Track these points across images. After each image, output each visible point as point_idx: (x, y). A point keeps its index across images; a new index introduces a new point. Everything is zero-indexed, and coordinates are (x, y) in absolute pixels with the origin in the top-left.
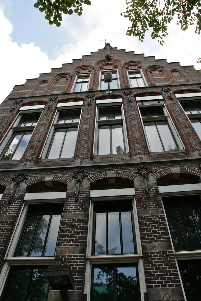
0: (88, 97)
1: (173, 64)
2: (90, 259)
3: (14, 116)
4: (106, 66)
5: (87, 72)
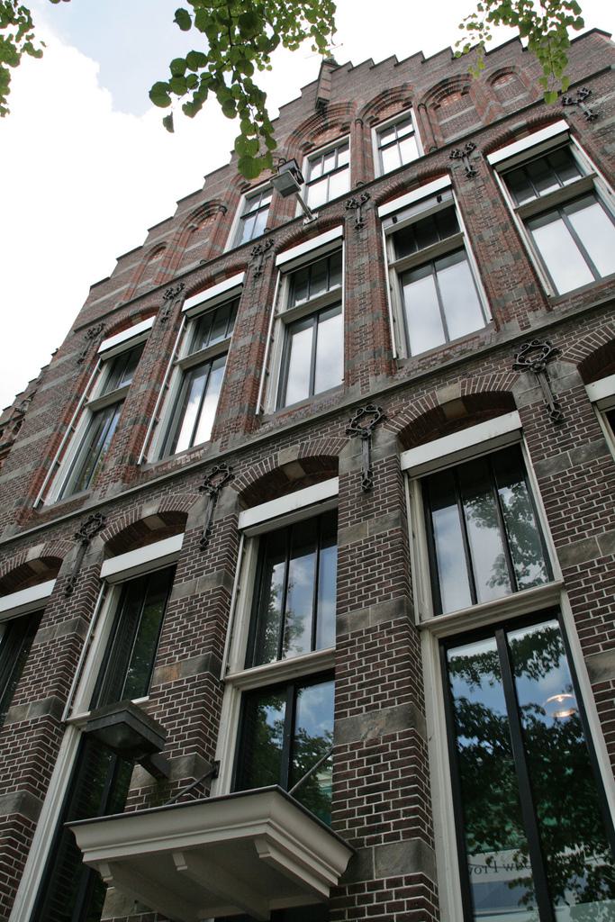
0: (352, 207)
1: (501, 51)
2: (429, 626)
3: (86, 375)
4: (321, 137)
5: (401, 109)
